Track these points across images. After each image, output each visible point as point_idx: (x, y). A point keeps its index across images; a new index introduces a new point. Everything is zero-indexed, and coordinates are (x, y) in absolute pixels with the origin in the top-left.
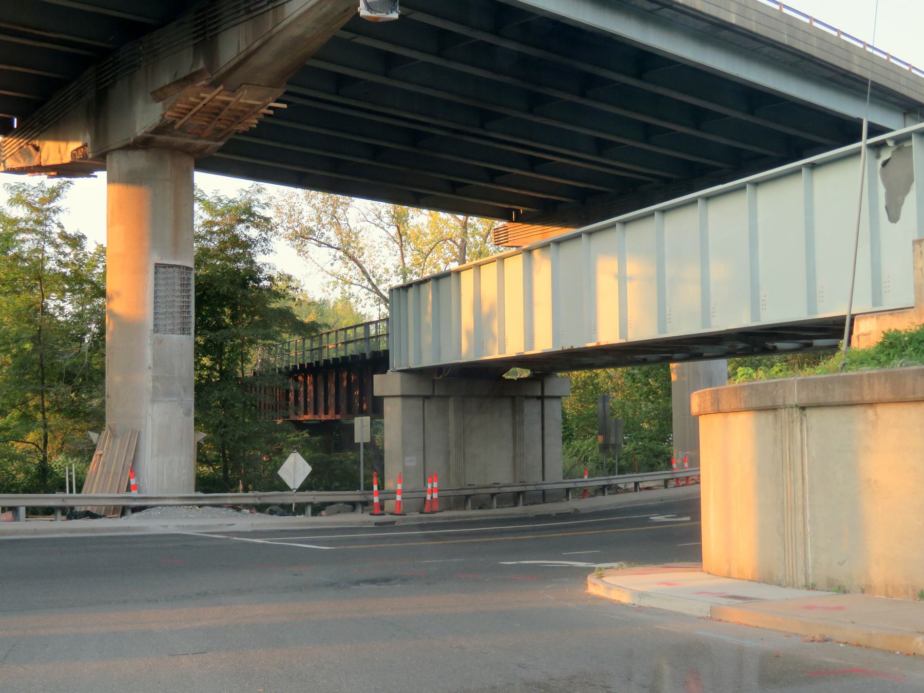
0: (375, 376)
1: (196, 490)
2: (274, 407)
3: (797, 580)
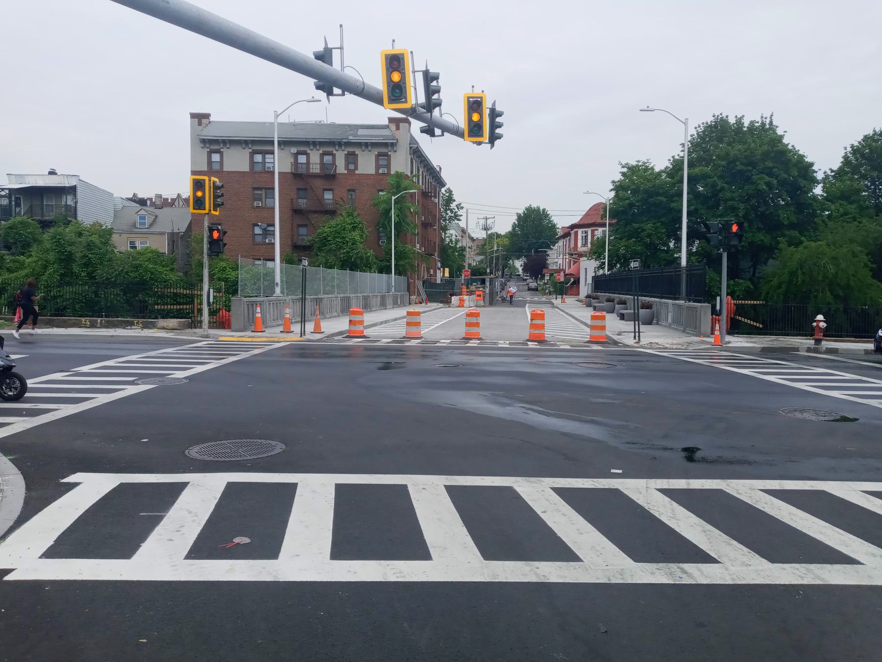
1: (405, 487)
2: (303, 334)
3: (415, 216)
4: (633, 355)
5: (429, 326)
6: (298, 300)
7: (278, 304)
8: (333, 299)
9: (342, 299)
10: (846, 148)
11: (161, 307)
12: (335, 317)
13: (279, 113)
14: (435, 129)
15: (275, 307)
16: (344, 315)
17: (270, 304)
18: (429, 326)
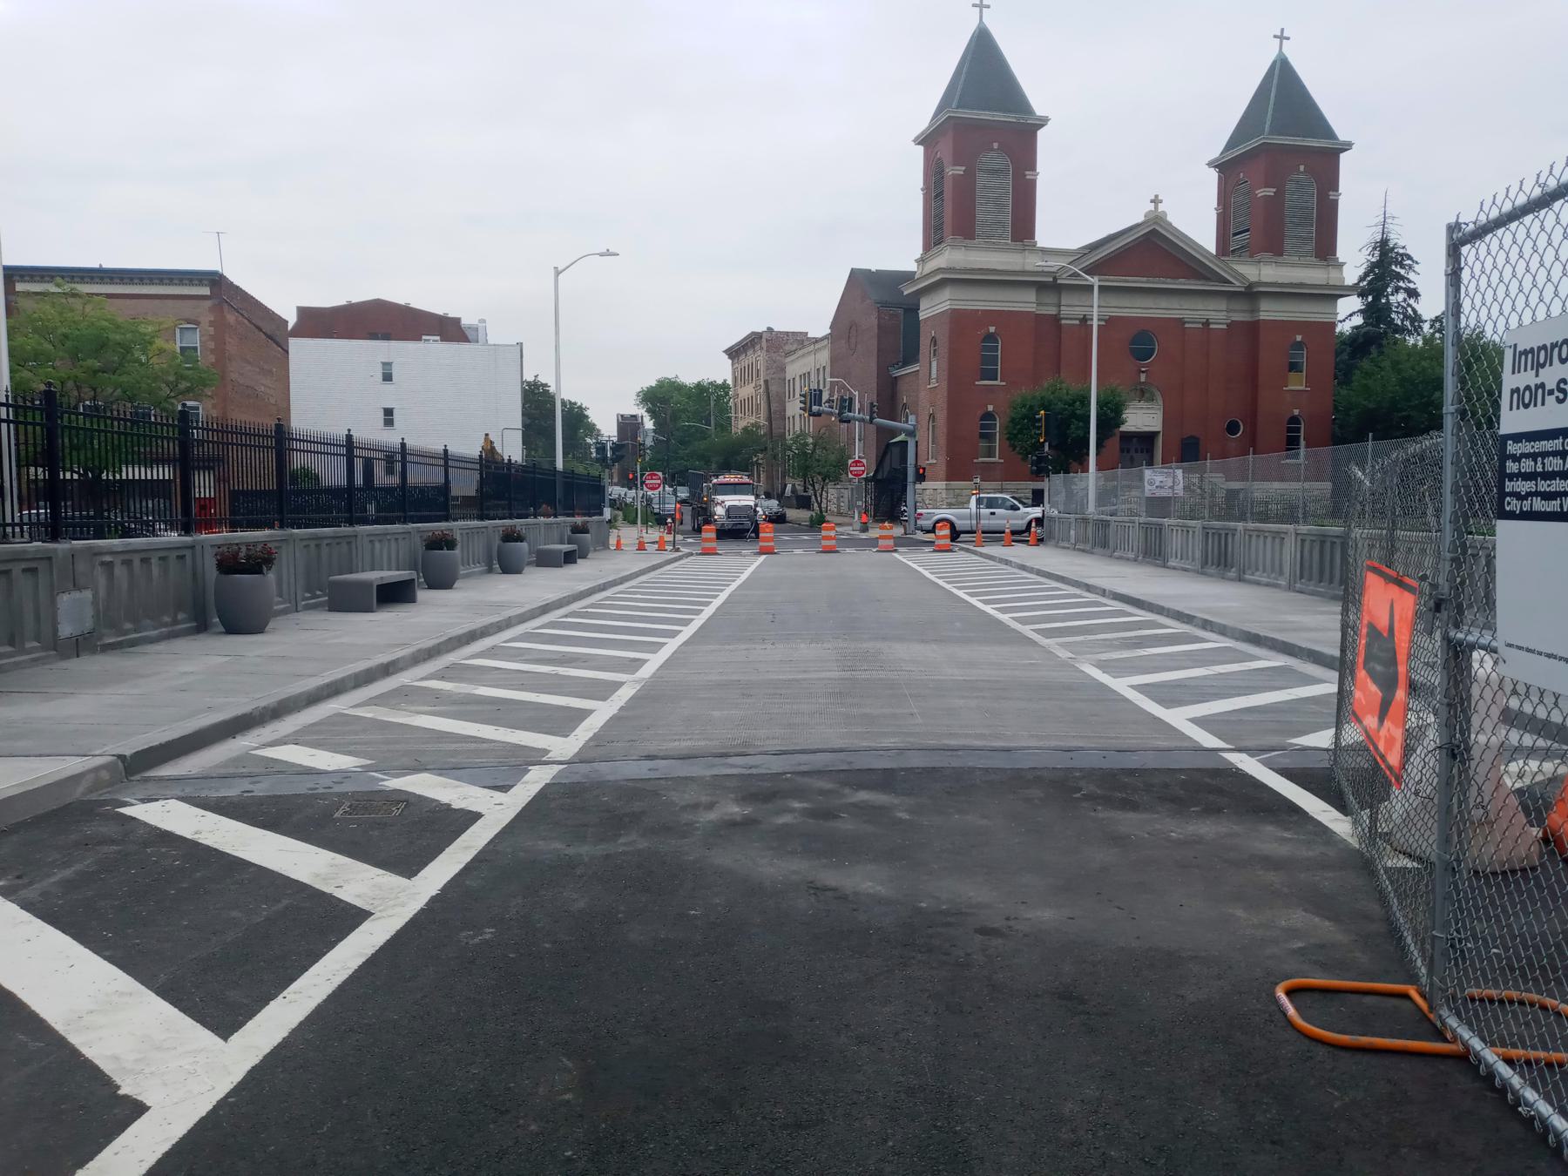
0: (17, 290)
1: (225, 1021)
4: (468, 703)
5: (729, 581)
6: (1101, 523)
7: (1180, 532)
8: (1127, 525)
9: (1146, 528)
10: (1404, 247)
11: (72, 476)
12: (1128, 559)
13: (560, 269)
14: (1214, 252)
15: (1190, 536)
16: (1148, 563)
17: (1250, 536)
18: (729, 581)
